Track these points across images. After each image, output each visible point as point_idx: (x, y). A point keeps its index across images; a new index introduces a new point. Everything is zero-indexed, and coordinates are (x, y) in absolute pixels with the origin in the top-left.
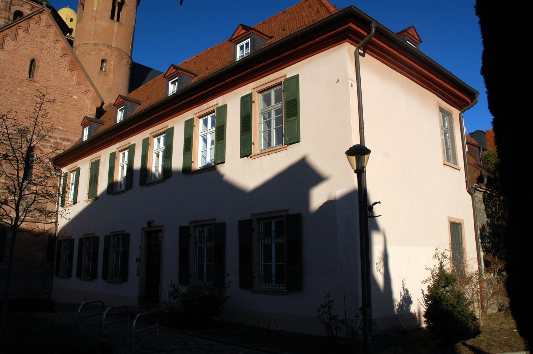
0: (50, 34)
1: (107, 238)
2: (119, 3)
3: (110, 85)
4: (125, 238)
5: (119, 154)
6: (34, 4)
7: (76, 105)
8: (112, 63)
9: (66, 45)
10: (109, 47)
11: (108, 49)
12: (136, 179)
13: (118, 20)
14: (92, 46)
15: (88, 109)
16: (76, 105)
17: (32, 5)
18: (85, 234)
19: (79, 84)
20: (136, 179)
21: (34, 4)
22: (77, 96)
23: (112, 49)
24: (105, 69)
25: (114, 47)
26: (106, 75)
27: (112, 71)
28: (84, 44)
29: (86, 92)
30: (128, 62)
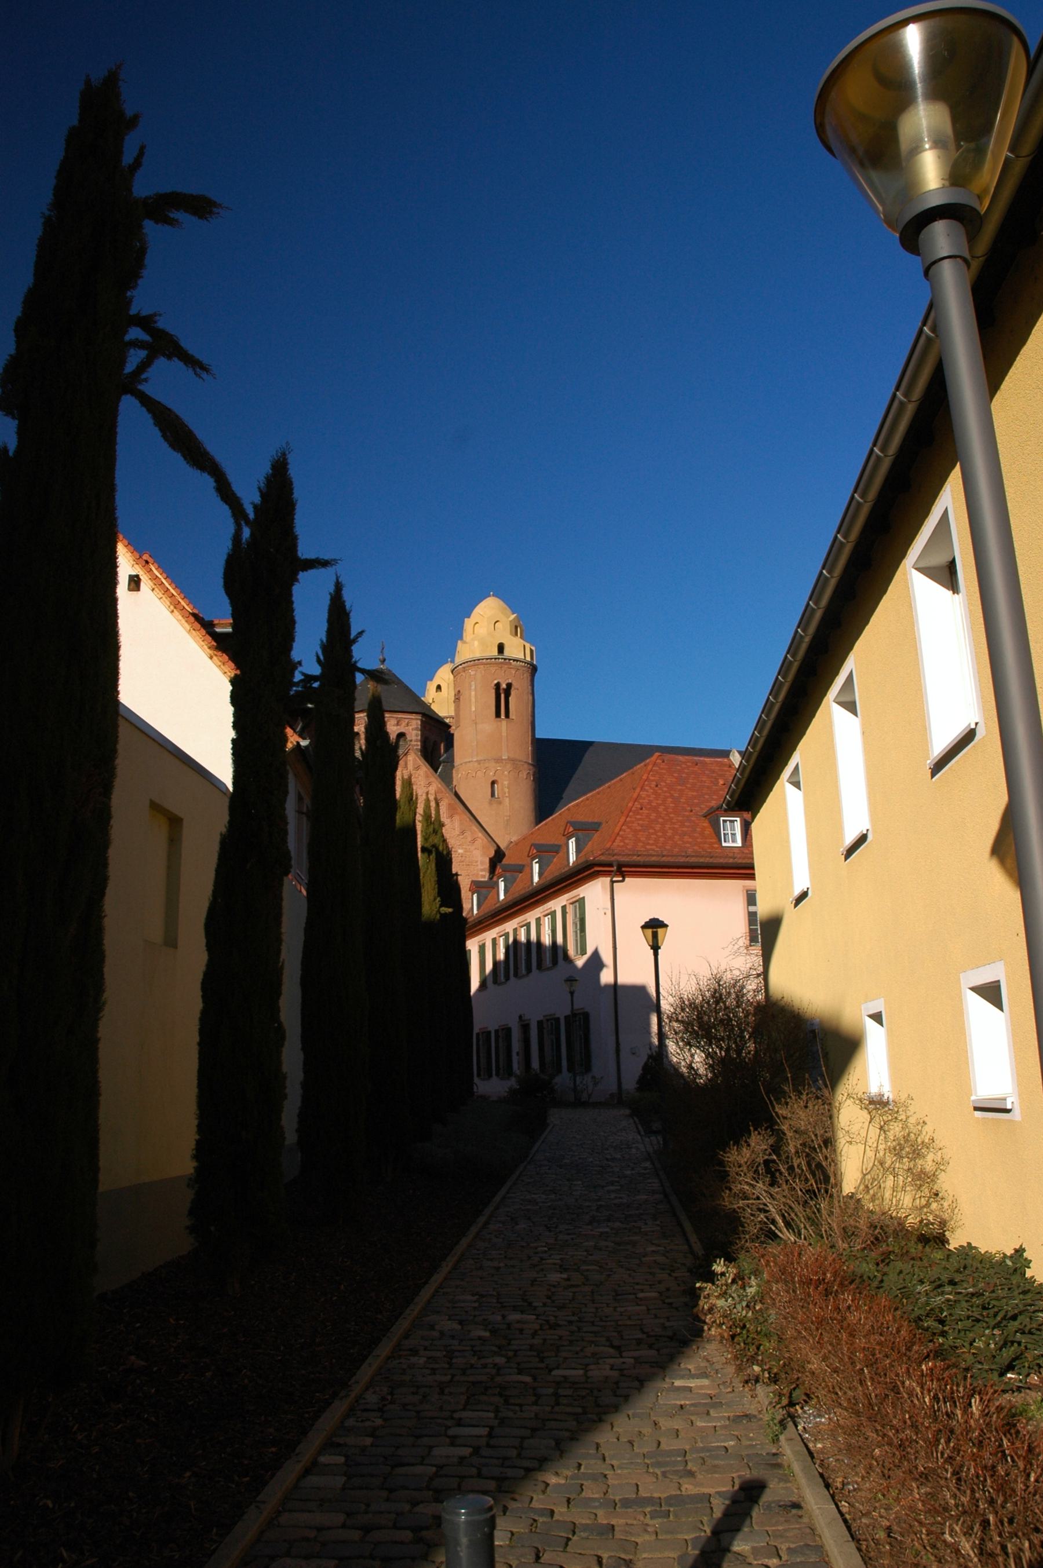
0: (420, 778)
1: (497, 1031)
2: (504, 689)
3: (507, 816)
4: (508, 1031)
5: (499, 940)
6: (399, 716)
7: (463, 862)
8: (506, 783)
9: (440, 786)
10: (498, 760)
11: (498, 765)
12: (490, 983)
13: (507, 716)
14: (476, 764)
15: (479, 863)
16: (463, 862)
17: (397, 718)
18: (546, 1016)
19: (463, 833)
20: (490, 983)
21: (399, 716)
22: (462, 849)
23: (502, 763)
24: (498, 795)
25: (505, 760)
26: (500, 803)
27: (507, 795)
28: (466, 763)
29: (474, 841)
30: (529, 773)
